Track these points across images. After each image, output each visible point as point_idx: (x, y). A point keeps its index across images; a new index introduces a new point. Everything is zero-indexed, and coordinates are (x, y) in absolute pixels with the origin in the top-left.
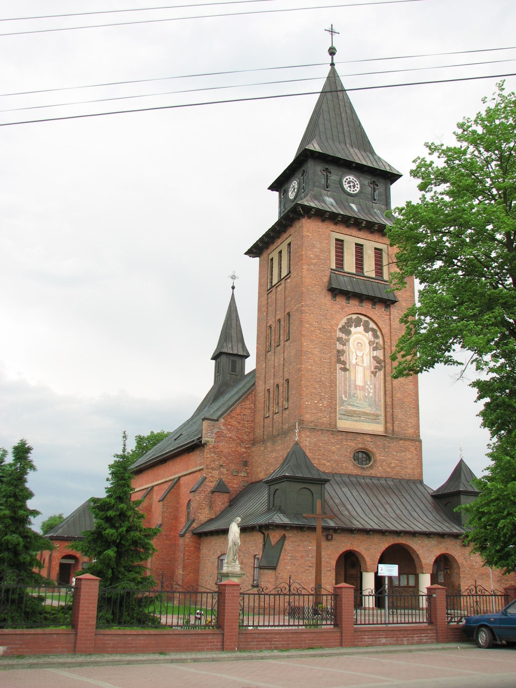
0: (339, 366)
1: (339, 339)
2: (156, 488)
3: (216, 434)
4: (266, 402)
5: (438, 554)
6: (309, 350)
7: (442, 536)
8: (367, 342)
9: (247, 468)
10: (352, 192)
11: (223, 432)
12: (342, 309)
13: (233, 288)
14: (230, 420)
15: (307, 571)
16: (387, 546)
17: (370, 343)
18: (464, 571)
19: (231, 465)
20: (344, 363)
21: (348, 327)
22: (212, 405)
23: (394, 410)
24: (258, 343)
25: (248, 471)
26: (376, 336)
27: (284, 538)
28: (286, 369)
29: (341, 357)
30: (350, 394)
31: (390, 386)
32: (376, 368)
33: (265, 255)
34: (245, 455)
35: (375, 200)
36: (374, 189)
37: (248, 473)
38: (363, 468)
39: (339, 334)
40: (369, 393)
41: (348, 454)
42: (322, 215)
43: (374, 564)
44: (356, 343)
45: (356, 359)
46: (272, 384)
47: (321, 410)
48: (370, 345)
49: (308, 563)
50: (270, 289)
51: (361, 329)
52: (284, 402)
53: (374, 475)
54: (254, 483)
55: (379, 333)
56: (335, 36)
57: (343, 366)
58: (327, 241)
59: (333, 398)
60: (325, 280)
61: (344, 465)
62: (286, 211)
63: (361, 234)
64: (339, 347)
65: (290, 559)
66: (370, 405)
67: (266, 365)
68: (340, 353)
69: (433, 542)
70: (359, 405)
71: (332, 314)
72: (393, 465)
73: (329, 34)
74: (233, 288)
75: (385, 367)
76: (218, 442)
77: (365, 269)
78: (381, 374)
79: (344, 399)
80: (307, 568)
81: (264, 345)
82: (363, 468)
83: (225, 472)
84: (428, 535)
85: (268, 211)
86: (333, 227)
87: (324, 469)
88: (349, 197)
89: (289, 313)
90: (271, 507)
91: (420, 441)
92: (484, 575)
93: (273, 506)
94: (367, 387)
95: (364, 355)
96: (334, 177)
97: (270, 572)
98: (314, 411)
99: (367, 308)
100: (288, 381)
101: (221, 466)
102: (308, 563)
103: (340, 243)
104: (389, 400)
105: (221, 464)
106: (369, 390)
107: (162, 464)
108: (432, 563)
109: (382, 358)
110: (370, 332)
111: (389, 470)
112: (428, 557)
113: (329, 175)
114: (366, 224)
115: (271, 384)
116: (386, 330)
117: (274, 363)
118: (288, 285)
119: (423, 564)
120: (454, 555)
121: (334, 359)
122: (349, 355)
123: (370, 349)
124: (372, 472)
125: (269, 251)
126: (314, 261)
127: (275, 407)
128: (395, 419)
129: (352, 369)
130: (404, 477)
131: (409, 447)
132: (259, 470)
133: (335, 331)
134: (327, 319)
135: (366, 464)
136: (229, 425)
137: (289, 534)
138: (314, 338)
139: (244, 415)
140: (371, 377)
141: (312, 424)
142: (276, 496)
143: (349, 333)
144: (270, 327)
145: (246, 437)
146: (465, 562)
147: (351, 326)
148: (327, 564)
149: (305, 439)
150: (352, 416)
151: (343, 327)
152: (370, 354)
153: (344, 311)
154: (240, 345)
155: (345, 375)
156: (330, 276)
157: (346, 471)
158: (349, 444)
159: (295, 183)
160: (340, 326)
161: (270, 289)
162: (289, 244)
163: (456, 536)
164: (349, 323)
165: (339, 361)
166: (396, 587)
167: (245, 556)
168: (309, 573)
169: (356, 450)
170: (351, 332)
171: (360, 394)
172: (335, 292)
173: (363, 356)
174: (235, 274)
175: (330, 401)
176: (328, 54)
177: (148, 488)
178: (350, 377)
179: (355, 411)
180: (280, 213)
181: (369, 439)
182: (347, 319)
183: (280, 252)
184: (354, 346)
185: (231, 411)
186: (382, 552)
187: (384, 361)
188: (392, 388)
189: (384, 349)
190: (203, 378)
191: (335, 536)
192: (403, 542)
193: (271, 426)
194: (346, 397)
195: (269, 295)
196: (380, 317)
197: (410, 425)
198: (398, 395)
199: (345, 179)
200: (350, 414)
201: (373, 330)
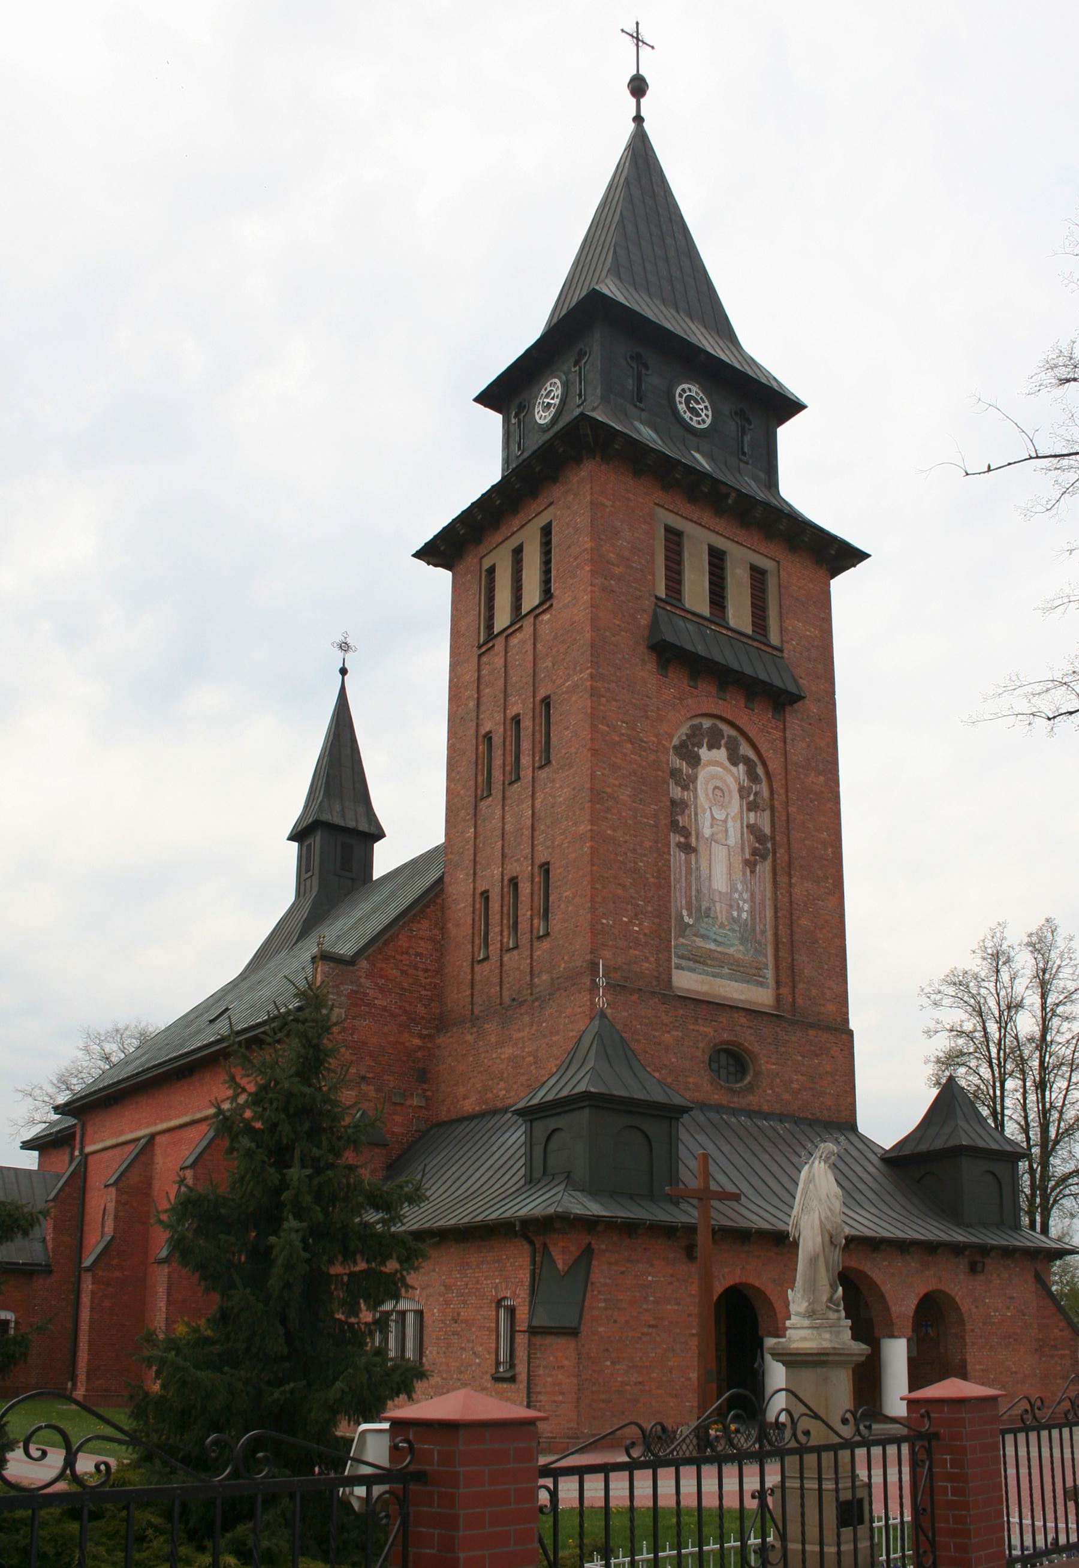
0: (675, 838)
1: (675, 773)
2: (161, 1140)
3: (348, 997)
4: (477, 925)
5: (923, 1291)
6: (609, 790)
7: (930, 1248)
8: (734, 788)
9: (426, 1086)
10: (694, 424)
12: (681, 699)
13: (343, 671)
14: (384, 966)
15: (645, 1339)
17: (743, 791)
18: (973, 1330)
19: (386, 1077)
20: (685, 832)
21: (694, 745)
22: (300, 945)
23: (796, 957)
24: (450, 778)
25: (428, 1093)
26: (753, 776)
27: (588, 1253)
28: (540, 838)
29: (679, 818)
30: (699, 909)
31: (786, 900)
32: (754, 852)
33: (470, 560)
34: (419, 1054)
35: (744, 454)
36: (743, 428)
37: (427, 1099)
39: (677, 762)
40: (740, 909)
41: (699, 1054)
42: (639, 461)
44: (711, 787)
45: (712, 826)
46: (498, 877)
48: (741, 797)
50: (485, 643)
51: (721, 754)
52: (536, 921)
53: (757, 1108)
54: (445, 1123)
55: (760, 770)
57: (682, 840)
58: (644, 527)
59: (663, 913)
60: (643, 622)
61: (691, 1080)
62: (526, 455)
64: (676, 792)
65: (606, 1308)
66: (743, 941)
67: (475, 832)
68: (678, 806)
70: (718, 938)
71: (658, 709)
72: (795, 1086)
73: (631, 43)
74: (343, 671)
75: (774, 853)
76: (354, 1018)
77: (731, 612)
78: (765, 868)
79: (686, 919)
80: (645, 1330)
81: (472, 783)
82: (733, 1091)
83: (373, 1094)
84: (902, 1246)
85: (474, 459)
88: (688, 436)
89: (548, 697)
90: (538, 1174)
91: (850, 1033)
92: (1010, 1337)
93: (545, 1173)
95: (730, 819)
96: (653, 380)
97: (561, 1341)
99: (733, 707)
100: (546, 868)
101: (363, 1078)
103: (674, 539)
104: (783, 931)
105: (363, 1073)
106: (741, 903)
107: (179, 1079)
108: (911, 1314)
109: (767, 831)
111: (786, 1096)
113: (644, 371)
115: (492, 877)
116: (775, 765)
117: (504, 824)
118: (544, 630)
119: (894, 1316)
120: (953, 1294)
121: (664, 821)
122: (696, 814)
123: (741, 806)
125: (482, 549)
126: (617, 571)
127: (505, 933)
128: (797, 978)
129: (702, 849)
131: (828, 1045)
132: (461, 1090)
133: (667, 750)
134: (647, 718)
135: (737, 1082)
136: (381, 977)
137: (599, 1245)
138: (619, 761)
139: (417, 954)
140: (744, 874)
142: (552, 1146)
143: (695, 761)
144: (488, 737)
145: (420, 1009)
146: (974, 1310)
147: (700, 746)
150: (704, 963)
152: (742, 819)
153: (679, 707)
154: (361, 810)
155: (688, 862)
156: (655, 610)
157: (696, 1094)
158: (702, 1029)
159: (553, 384)
160: (675, 741)
161: (485, 643)
162: (547, 531)
163: (957, 1249)
164: (695, 736)
167: (465, 1302)
170: (700, 759)
171: (720, 910)
172: (667, 654)
173: (725, 821)
174: (348, 641)
175: (656, 920)
176: (628, 92)
177: (138, 1139)
178: (698, 869)
179: (711, 950)
180: (506, 461)
181: (743, 1020)
182: (692, 726)
183: (518, 551)
184: (707, 795)
185: (386, 943)
187: (773, 838)
188: (791, 902)
189: (772, 809)
190: (270, 880)
193: (496, 980)
194: (690, 916)
195: (485, 659)
198: (804, 922)
199: (679, 391)
200: (699, 960)
201: (747, 761)
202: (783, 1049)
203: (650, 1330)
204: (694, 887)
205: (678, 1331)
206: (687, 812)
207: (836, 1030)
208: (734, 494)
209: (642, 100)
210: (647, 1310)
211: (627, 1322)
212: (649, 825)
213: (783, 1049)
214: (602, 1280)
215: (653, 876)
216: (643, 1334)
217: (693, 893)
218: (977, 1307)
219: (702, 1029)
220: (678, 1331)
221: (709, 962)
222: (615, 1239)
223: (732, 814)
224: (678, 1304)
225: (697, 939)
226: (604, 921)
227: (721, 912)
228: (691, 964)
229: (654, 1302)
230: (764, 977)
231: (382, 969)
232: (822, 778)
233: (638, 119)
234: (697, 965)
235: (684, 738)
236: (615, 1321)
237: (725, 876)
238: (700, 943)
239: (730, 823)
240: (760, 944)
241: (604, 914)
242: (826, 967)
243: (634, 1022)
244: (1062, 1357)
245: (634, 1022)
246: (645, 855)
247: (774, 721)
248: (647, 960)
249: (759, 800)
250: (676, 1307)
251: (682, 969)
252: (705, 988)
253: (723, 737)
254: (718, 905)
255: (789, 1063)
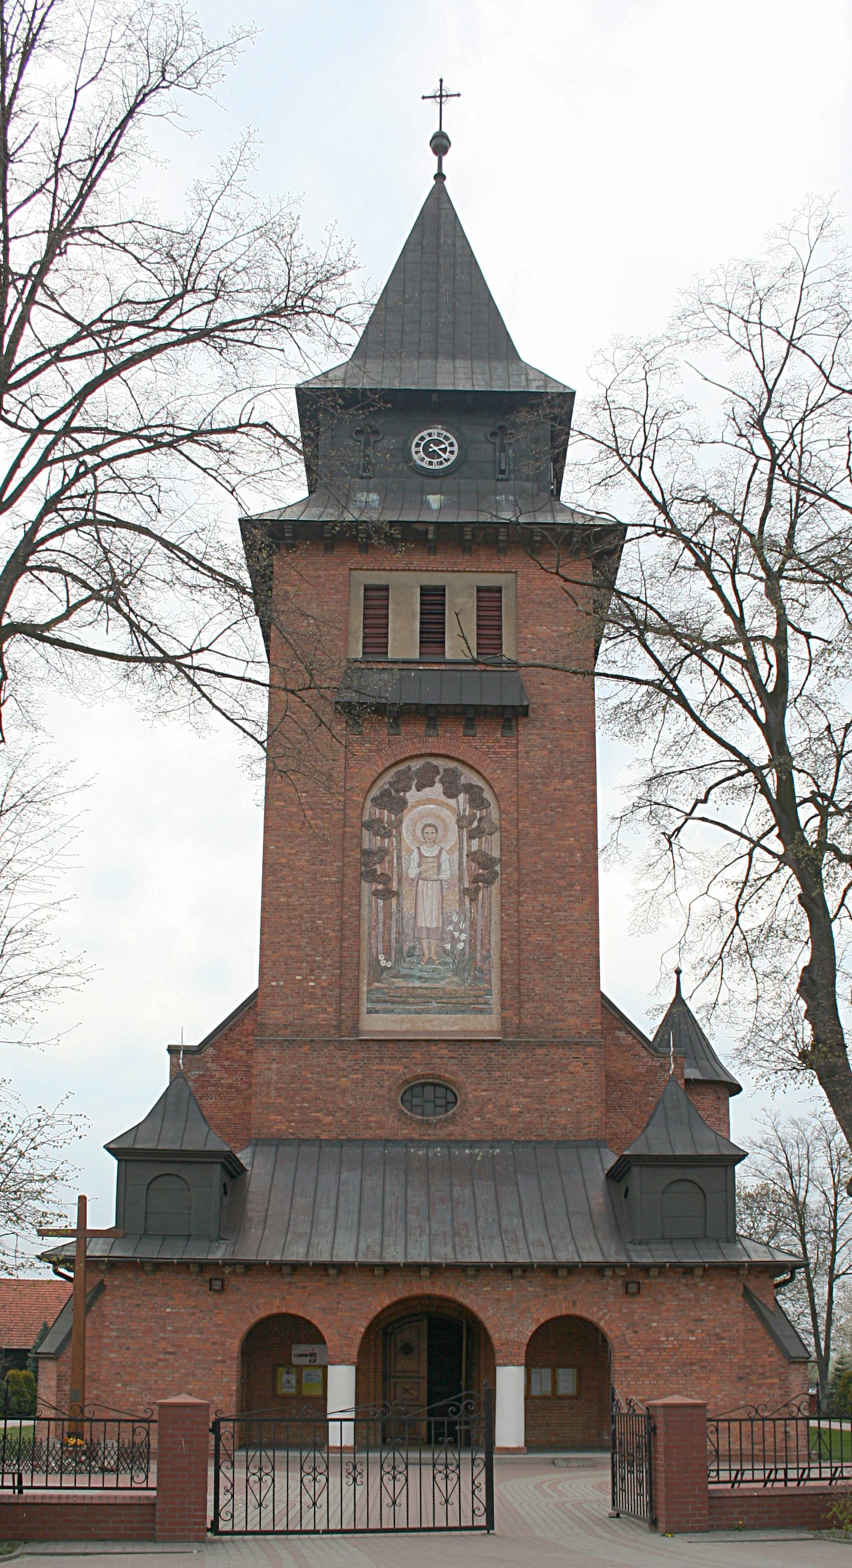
0: (366, 888)
1: (371, 825)
6: (284, 861)
10: (435, 467)
11: (212, 1076)
14: (230, 1049)
15: (160, 1364)
16: (387, 1302)
17: (461, 821)
20: (386, 879)
26: (476, 800)
32: (475, 880)
38: (428, 1123)
39: (371, 812)
40: (454, 941)
41: (384, 1092)
43: (349, 1346)
44: (419, 827)
45: (419, 865)
47: (312, 996)
48: (460, 827)
49: (163, 1344)
55: (487, 795)
56: (450, 104)
61: (373, 1119)
63: (436, 560)
64: (370, 841)
65: (118, 1337)
69: (532, 1286)
70: (425, 975)
72: (514, 1109)
79: (383, 963)
80: (161, 1356)
82: (428, 1123)
86: (356, 559)
87: (318, 1132)
92: (692, 1364)
94: (451, 928)
95: (444, 852)
98: (292, 1001)
102: (163, 1344)
106: (456, 934)
108: (526, 1341)
110: (462, 797)
112: (514, 1326)
114: (437, 532)
122: (399, 858)
123: (460, 837)
124: (454, 1131)
129: (406, 890)
130: (548, 1135)
136: (227, 1059)
140: (461, 903)
141: (289, 1031)
143: (402, 804)
146: (629, 1334)
147: (407, 789)
148: (215, 1347)
149: (266, 1066)
150: (405, 1003)
151: (385, 793)
152: (461, 849)
155: (387, 908)
165: (371, 876)
166: (287, 1397)
168: (166, 1367)
169: (407, 1082)
171: (429, 947)
173: (439, 856)
178: (399, 911)
181: (444, 1052)
184: (414, 836)
185: (230, 1029)
186: (371, 1317)
191: (234, 1282)
192: (437, 1291)
194: (387, 960)
196: (486, 754)
197: (569, 1007)
200: (397, 1001)
201: (469, 789)
202: (498, 1074)
203: (167, 1356)
204: (394, 930)
205: (200, 1357)
206: (387, 858)
207: (577, 1044)
208: (431, 528)
209: (444, 158)
210: (163, 1339)
211: (141, 1349)
212: (331, 882)
213: (498, 1074)
214: (114, 1312)
215: (334, 930)
216: (159, 1360)
217: (393, 936)
218: (635, 1332)
219: (388, 1067)
220: (200, 1357)
221: (411, 1000)
222: (130, 1276)
223: (448, 848)
224: (202, 1333)
225: (396, 980)
226: (274, 984)
227: (429, 948)
228: (389, 1006)
229: (172, 1331)
230: (486, 1003)
231: (228, 1052)
232: (569, 782)
233: (440, 177)
234: (396, 1006)
235: (387, 786)
236: (128, 1348)
237: (435, 913)
238: (399, 983)
239: (444, 856)
240: (481, 971)
241: (274, 977)
242: (568, 979)
243: (304, 1073)
244: (771, 1386)
245: (304, 1073)
246: (325, 913)
247: (503, 740)
248: (324, 1011)
249: (484, 825)
250: (198, 1336)
251: (377, 1012)
252: (406, 1027)
253: (438, 773)
254: (425, 943)
255: (507, 1087)
